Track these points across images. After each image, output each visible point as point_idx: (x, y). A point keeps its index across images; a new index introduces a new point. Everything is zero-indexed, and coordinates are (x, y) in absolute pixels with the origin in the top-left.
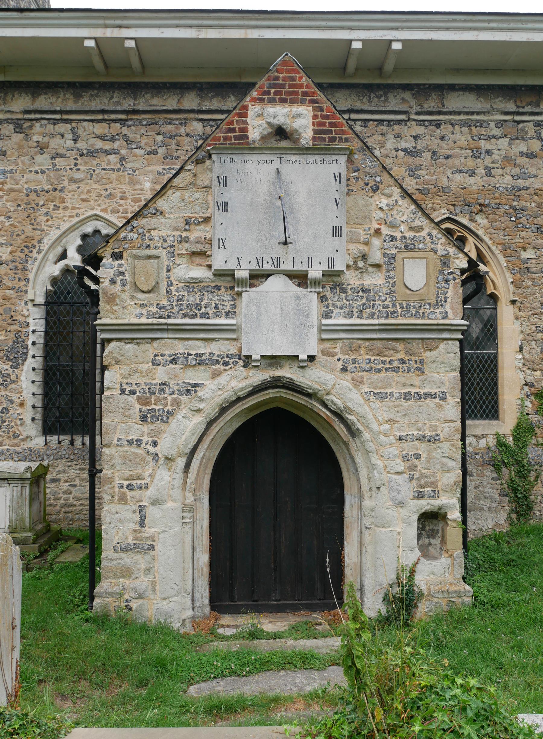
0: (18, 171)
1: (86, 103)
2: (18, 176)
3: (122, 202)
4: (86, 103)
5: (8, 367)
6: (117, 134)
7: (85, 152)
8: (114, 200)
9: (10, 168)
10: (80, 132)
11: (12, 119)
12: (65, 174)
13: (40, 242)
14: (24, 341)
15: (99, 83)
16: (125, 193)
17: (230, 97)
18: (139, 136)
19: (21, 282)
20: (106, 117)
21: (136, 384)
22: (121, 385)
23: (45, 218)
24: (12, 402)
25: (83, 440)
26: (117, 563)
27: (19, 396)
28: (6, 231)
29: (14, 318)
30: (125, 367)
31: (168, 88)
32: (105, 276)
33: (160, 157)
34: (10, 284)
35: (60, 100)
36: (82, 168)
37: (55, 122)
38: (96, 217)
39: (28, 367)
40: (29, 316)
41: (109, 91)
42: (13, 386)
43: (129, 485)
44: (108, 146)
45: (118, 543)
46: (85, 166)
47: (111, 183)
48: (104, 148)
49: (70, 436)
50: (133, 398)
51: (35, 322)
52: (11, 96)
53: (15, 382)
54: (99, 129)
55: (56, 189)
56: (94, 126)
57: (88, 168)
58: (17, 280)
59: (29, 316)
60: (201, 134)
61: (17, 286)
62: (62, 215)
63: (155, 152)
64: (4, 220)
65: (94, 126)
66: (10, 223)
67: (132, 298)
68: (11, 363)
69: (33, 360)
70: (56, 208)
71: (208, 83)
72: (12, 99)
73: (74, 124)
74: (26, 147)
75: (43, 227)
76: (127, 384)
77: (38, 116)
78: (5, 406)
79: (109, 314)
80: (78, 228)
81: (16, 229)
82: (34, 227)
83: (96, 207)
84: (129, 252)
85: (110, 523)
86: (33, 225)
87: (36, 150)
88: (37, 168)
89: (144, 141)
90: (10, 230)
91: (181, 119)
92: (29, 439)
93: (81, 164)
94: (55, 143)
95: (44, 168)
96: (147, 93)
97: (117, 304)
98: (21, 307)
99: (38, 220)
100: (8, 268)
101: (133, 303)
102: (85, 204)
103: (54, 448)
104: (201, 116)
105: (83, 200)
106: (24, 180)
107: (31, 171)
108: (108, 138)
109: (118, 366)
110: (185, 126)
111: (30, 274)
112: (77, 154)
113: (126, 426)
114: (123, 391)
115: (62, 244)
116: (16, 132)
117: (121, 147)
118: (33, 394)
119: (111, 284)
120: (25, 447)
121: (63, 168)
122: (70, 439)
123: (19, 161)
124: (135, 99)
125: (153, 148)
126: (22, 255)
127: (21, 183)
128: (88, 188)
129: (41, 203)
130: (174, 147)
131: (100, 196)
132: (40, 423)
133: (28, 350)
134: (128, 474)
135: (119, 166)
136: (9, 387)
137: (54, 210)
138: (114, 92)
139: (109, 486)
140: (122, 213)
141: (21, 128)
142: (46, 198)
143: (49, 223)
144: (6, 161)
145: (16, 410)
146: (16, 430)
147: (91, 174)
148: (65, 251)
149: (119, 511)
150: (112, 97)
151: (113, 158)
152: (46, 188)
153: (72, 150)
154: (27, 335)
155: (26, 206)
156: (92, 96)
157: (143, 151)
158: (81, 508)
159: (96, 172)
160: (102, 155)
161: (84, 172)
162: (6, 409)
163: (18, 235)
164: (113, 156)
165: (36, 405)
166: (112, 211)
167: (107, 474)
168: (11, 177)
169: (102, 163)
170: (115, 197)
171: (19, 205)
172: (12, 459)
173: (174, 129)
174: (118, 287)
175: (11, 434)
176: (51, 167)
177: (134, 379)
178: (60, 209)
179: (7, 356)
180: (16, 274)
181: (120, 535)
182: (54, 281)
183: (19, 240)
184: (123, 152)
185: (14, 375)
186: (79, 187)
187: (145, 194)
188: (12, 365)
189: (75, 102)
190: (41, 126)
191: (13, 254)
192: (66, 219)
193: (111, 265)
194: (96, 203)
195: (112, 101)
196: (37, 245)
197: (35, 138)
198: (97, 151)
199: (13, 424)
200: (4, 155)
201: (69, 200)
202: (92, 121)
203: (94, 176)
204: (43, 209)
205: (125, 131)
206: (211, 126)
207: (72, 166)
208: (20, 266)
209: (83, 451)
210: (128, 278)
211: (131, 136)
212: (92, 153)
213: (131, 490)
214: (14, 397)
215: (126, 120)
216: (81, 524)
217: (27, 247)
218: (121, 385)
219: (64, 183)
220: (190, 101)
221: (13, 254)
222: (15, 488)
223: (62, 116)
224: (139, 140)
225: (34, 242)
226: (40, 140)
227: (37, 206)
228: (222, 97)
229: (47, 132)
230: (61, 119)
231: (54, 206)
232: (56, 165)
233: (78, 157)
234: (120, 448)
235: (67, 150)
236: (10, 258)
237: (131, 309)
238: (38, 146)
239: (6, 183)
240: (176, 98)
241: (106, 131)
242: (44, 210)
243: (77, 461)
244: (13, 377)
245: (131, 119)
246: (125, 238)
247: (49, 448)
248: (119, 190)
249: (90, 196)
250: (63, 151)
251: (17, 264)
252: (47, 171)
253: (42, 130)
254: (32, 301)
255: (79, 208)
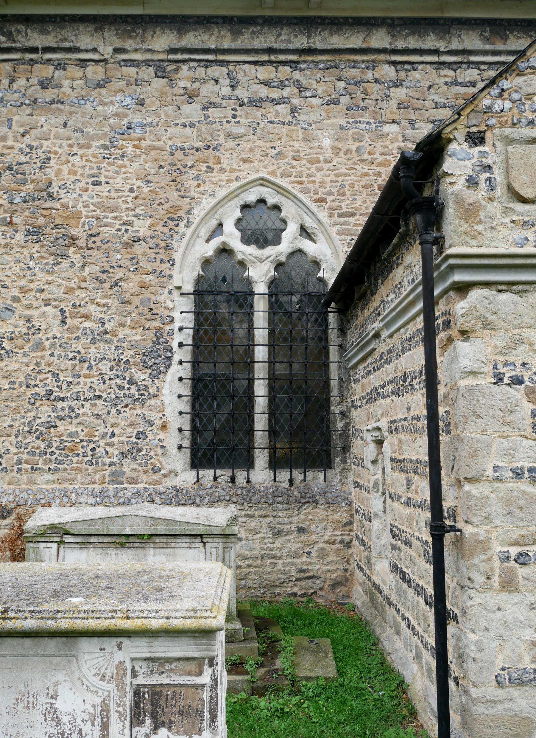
0: (160, 124)
1: (246, 41)
2: (160, 130)
3: (295, 163)
4: (246, 41)
5: (146, 376)
6: (287, 80)
7: (246, 100)
8: (285, 161)
9: (149, 120)
10: (240, 76)
11: (153, 61)
12: (220, 127)
13: (189, 212)
14: (167, 342)
15: (262, 17)
16: (298, 151)
17: (429, 35)
18: (315, 82)
19: (163, 265)
20: (273, 58)
21: (524, 364)
22: (495, 367)
23: (196, 183)
24: (151, 423)
25: (248, 475)
26: (505, 710)
27: (160, 415)
28: (144, 199)
29: (154, 311)
30: (500, 333)
31: (351, 25)
32: (457, 173)
33: (342, 107)
34: (149, 267)
35: (213, 37)
36: (243, 121)
37: (208, 64)
38: (261, 182)
39: (173, 377)
40: (173, 309)
41: (276, 28)
42: (152, 402)
43: (520, 554)
44: (275, 94)
45: (503, 669)
46: (246, 118)
47: (280, 139)
48: (270, 96)
49: (231, 471)
50: (518, 391)
51: (182, 315)
52: (151, 33)
53: (155, 396)
54: (264, 73)
55: (209, 147)
56: (256, 70)
57: (250, 120)
58: (158, 261)
59: (173, 309)
60: (394, 79)
61: (158, 270)
62: (217, 179)
63: (335, 102)
64: (142, 185)
65: (256, 70)
66: (149, 189)
67: (507, 211)
68: (149, 371)
69: (180, 367)
70: (210, 169)
71: (401, 18)
72: (153, 37)
73: (231, 68)
74: (170, 94)
75: (193, 194)
76: (506, 364)
77: (186, 56)
78: (141, 429)
79: (468, 239)
80: (237, 196)
81: (158, 197)
82: (182, 194)
83: (261, 169)
84: (497, 131)
85: (487, 630)
86: (179, 191)
87: (183, 98)
88: (184, 121)
89: (321, 89)
90: (150, 197)
91: (368, 61)
92: (173, 475)
93: (241, 116)
94: (208, 91)
95: (193, 120)
96: (323, 30)
97: (481, 222)
98: (163, 297)
99: (186, 185)
100: (147, 246)
101: (507, 220)
102: (248, 165)
103: (209, 486)
104: (394, 58)
105: (245, 161)
106: (168, 135)
107: (177, 124)
108: (276, 84)
109: (488, 332)
110: (373, 70)
111: (175, 253)
112: (236, 104)
113: (506, 444)
114: (499, 378)
115: (217, 216)
116: (157, 76)
117: (293, 95)
118: (180, 413)
119: (468, 187)
120: (168, 485)
121: (217, 120)
122: (231, 474)
123: (161, 112)
124: (309, 37)
125: (333, 96)
126: (166, 230)
127: (164, 139)
128: (250, 145)
129: (190, 164)
130: (360, 95)
131: (266, 155)
132: (188, 451)
133: (172, 353)
134: (515, 534)
135: (289, 118)
136: (147, 404)
137: (207, 172)
138: (282, 29)
139: (483, 557)
140: (296, 177)
141: (164, 72)
142: (196, 158)
143: (201, 189)
144: (144, 111)
145: (157, 434)
146: (156, 462)
147: (254, 127)
148: (220, 225)
149: (502, 605)
150: (280, 35)
151: (282, 109)
152: (196, 145)
153: (230, 99)
154: (171, 334)
155: (170, 168)
156: (254, 32)
157: (321, 100)
158: (249, 570)
159: (261, 126)
160: (267, 104)
161: (245, 125)
162: (143, 433)
163: (161, 204)
164: (283, 106)
165: (184, 428)
166: (282, 175)
167: (477, 534)
168: (151, 132)
169: (269, 115)
170: (286, 157)
171: (161, 167)
172: (153, 501)
173: (359, 74)
174: (482, 191)
175: (150, 467)
176: (203, 119)
177: (519, 355)
178: (215, 171)
179: (145, 362)
180: (157, 253)
181: (507, 652)
182: (206, 263)
183: (161, 211)
184: (296, 101)
185: (154, 387)
186: (238, 145)
187: (324, 153)
188: (150, 374)
189: (233, 40)
190: (190, 69)
191: (154, 228)
192: (223, 183)
193: (467, 153)
194: (261, 165)
195: (280, 39)
196: (185, 217)
197: (182, 84)
198: (262, 100)
199: (152, 453)
200: (142, 105)
201: (226, 161)
202: (255, 63)
203: (258, 131)
204: (193, 172)
205: (297, 75)
206: (406, 70)
207: (230, 119)
208: (163, 244)
209: (249, 491)
210: (498, 175)
211: (305, 82)
212: (255, 103)
213: (524, 564)
214: (154, 416)
215: (298, 62)
216: (248, 593)
217: (172, 219)
218: (495, 367)
219: (220, 138)
220: (379, 39)
221: (154, 228)
222: (214, 550)
223: (216, 56)
224: (315, 87)
225: (182, 213)
226: (189, 86)
227: (185, 168)
228: (420, 36)
229: (197, 77)
230: (215, 61)
231: (207, 167)
232: (209, 117)
233: (238, 107)
234: (499, 485)
235: (223, 99)
236: (149, 233)
237: (505, 232)
238: (186, 94)
239: (144, 139)
240: (361, 36)
241: (273, 76)
242: (193, 173)
243: (242, 504)
244: (152, 390)
245: (305, 62)
246: (488, 110)
247: (201, 487)
248: (291, 148)
249: (253, 155)
250: (218, 100)
251: (158, 241)
252: (197, 124)
253: (191, 74)
254: (179, 288)
255: (239, 171)
